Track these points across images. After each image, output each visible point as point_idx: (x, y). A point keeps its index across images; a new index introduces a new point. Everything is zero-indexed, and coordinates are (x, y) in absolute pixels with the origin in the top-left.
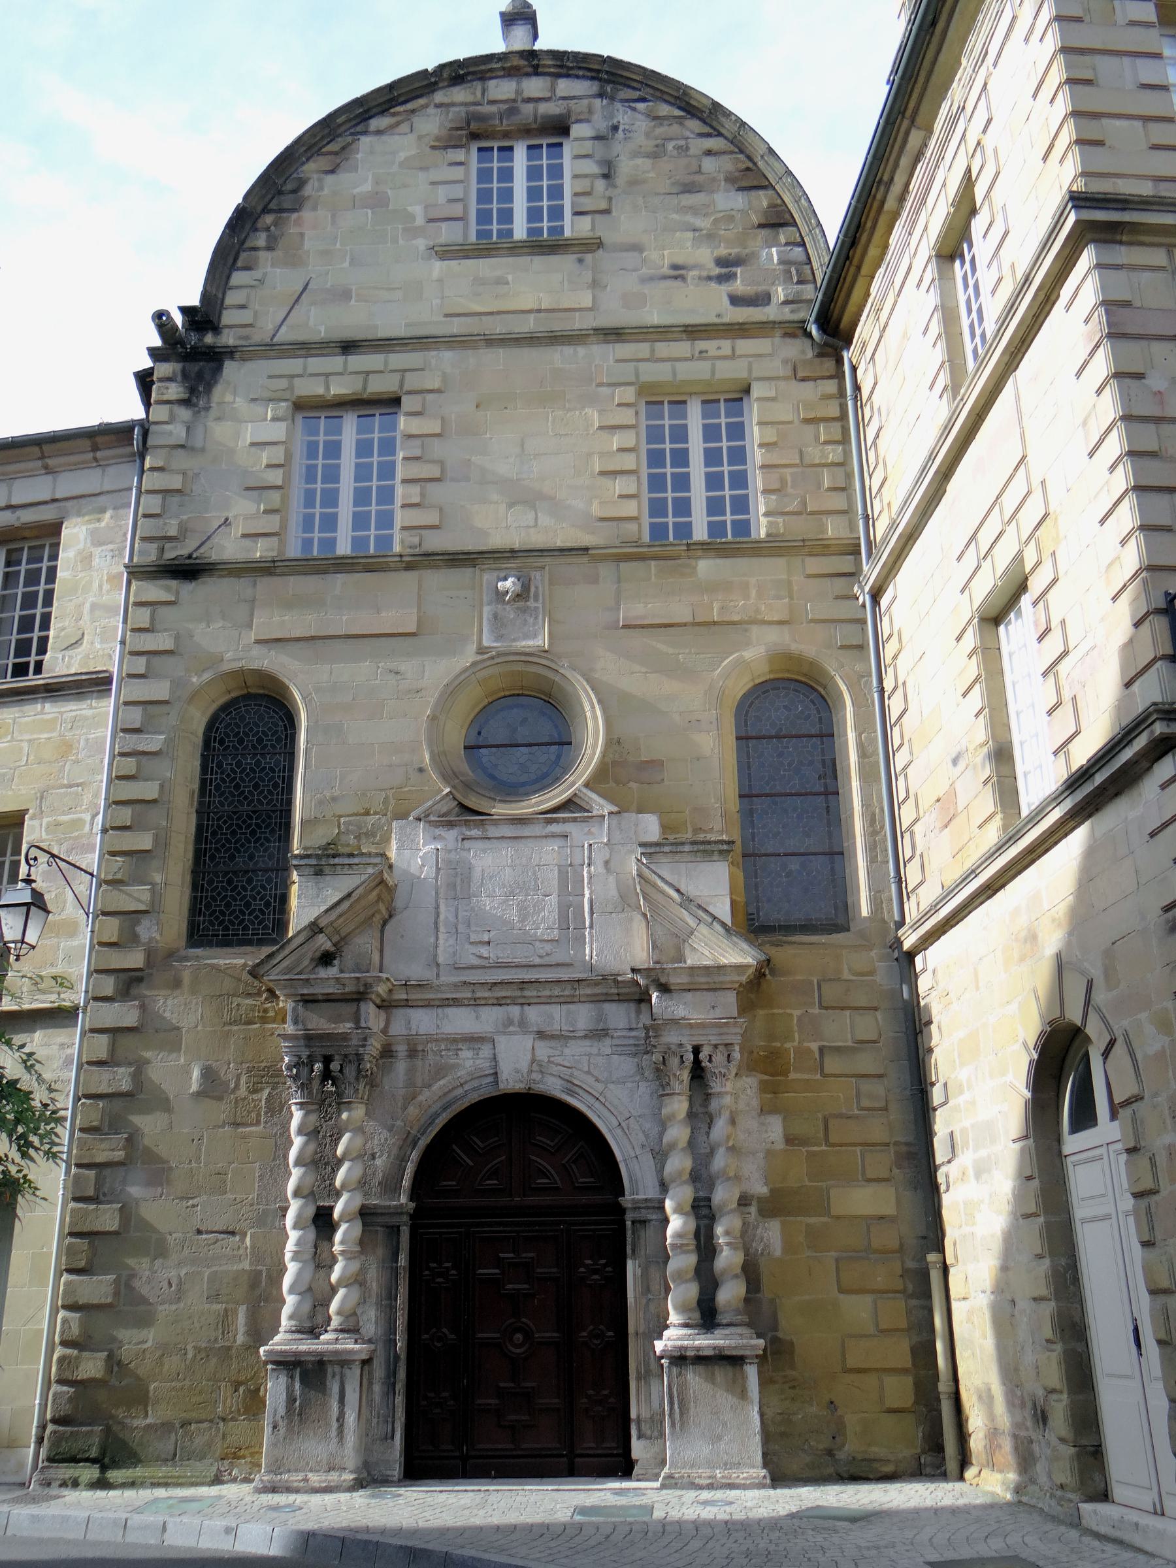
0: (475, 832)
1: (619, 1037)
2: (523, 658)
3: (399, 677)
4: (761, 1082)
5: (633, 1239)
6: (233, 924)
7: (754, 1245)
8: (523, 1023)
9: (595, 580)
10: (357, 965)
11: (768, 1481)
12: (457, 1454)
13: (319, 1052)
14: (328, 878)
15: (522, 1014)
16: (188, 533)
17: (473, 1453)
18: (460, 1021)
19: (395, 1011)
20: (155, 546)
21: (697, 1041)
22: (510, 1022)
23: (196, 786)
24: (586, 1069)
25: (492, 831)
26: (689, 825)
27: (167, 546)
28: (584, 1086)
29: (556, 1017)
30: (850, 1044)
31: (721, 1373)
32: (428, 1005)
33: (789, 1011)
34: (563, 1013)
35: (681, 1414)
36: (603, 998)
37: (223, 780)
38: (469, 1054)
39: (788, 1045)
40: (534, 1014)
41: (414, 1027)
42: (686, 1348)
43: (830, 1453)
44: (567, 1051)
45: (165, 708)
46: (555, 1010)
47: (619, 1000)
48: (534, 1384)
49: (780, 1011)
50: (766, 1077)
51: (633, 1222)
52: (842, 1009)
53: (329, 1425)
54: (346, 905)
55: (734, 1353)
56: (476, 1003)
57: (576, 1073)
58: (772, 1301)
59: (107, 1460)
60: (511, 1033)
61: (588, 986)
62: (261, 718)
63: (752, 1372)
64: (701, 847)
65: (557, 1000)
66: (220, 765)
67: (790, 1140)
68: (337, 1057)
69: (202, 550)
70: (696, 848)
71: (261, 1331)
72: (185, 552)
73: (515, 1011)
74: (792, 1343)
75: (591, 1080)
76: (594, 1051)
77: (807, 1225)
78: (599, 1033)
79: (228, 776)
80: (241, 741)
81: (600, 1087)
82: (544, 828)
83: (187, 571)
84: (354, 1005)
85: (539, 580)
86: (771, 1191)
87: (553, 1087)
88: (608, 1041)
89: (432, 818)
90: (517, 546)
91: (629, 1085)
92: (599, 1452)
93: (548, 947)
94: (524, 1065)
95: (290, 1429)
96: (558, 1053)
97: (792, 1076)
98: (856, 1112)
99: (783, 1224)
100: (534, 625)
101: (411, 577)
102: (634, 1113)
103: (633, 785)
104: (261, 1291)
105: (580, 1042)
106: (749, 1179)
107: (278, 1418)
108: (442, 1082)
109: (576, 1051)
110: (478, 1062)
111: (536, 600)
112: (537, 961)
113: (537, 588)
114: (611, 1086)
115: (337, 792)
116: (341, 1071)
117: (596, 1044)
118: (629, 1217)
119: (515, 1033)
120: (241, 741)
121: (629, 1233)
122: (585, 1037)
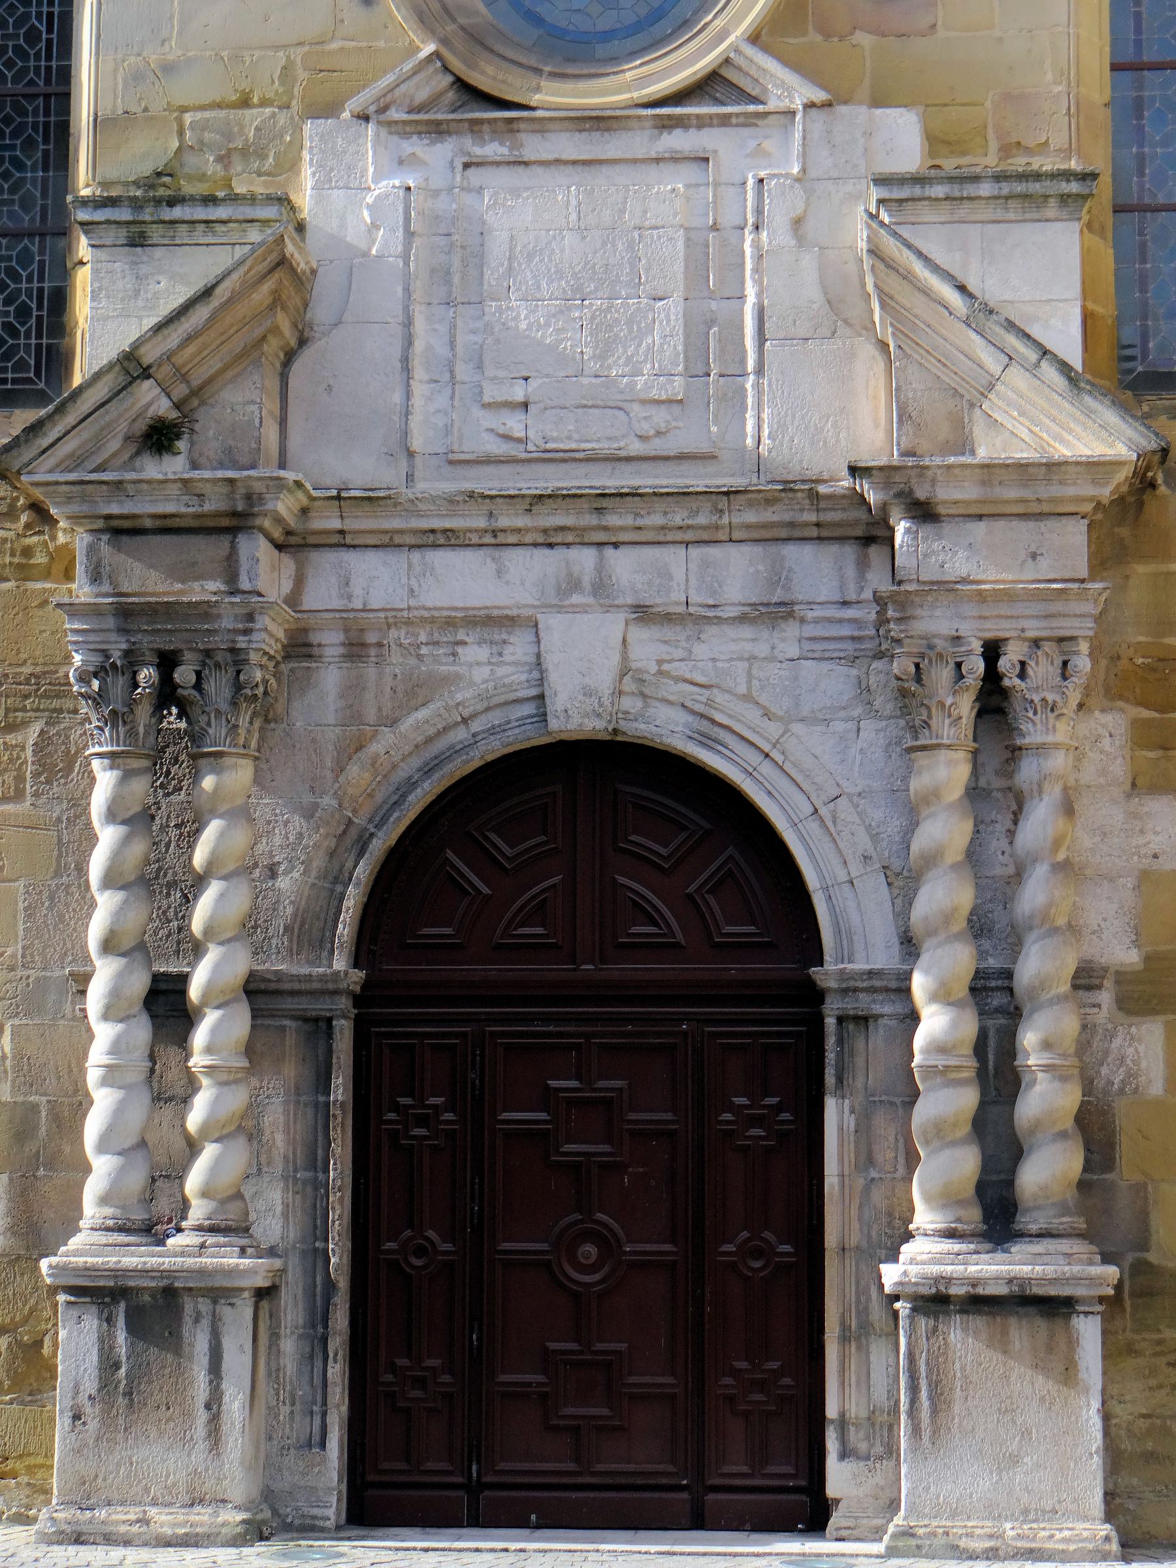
0: (493, 149)
1: (816, 621)
4: (1138, 725)
7: (1104, 1071)
8: (601, 587)
10: (229, 451)
11: (1115, 1547)
12: (459, 1480)
13: (147, 643)
14: (159, 252)
15: (600, 567)
17: (485, 1479)
18: (462, 580)
19: (315, 556)
22: (574, 585)
24: (742, 689)
29: (677, 573)
31: (1022, 1332)
32: (388, 543)
35: (935, 1411)
40: (625, 566)
41: (357, 590)
42: (949, 1280)
46: (675, 559)
47: (820, 539)
50: (1146, 714)
51: (840, 1020)
54: (201, 314)
55: (1053, 1292)
56: (496, 540)
57: (719, 698)
58: (1140, 1189)
61: (751, 504)
63: (1088, 1331)
64: (1020, 188)
65: (680, 536)
68: (188, 656)
70: (1006, 188)
73: (584, 559)
75: (753, 715)
76: (762, 649)
78: (774, 612)
81: (773, 729)
84: (225, 541)
86: (1148, 959)
87: (667, 728)
88: (792, 630)
89: (395, 114)
91: (839, 726)
93: (660, 417)
96: (680, 653)
99: (1167, 1024)
103: (864, 39)
105: (730, 631)
106: (1098, 932)
107: (83, 1398)
108: (422, 714)
109: (720, 649)
110: (501, 671)
112: (636, 448)
114: (797, 728)
116: (198, 686)
117: (765, 634)
118: (832, 1009)
119: (584, 609)
121: (831, 1042)
122: (742, 619)
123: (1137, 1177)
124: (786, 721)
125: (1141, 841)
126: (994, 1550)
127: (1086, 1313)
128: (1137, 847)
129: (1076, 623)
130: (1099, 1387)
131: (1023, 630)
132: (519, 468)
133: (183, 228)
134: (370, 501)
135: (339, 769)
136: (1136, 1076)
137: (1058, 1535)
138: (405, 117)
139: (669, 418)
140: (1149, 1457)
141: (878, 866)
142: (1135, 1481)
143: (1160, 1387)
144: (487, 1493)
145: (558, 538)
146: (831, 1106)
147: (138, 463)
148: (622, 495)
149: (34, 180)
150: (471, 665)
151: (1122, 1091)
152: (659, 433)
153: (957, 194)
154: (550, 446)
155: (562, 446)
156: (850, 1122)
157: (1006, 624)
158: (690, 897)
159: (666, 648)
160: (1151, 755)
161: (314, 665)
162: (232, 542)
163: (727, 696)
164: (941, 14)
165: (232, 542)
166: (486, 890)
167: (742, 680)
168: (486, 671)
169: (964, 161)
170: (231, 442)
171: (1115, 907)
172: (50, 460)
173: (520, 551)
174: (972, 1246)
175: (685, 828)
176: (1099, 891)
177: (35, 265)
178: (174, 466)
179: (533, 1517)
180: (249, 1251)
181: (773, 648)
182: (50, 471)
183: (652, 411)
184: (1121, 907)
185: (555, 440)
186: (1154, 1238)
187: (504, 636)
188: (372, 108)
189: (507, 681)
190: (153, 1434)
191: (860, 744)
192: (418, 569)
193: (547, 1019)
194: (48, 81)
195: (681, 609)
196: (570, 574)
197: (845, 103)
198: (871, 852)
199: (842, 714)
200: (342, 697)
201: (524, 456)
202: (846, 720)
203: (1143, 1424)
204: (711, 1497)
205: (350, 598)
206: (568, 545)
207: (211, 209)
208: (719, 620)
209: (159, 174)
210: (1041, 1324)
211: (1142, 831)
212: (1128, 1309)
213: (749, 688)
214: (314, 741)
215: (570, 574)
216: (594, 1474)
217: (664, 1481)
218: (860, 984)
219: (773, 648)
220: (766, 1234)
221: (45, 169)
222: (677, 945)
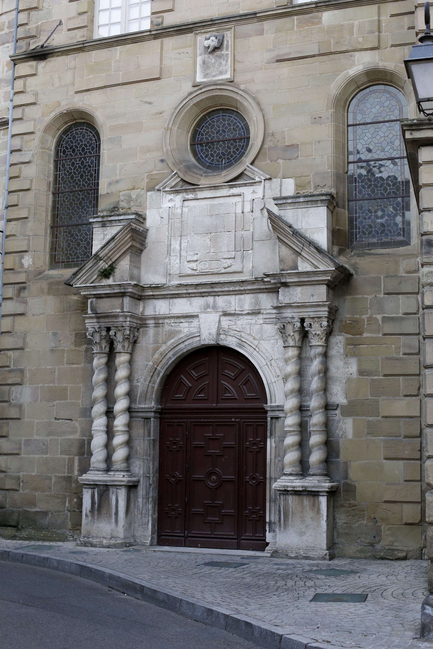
0: (191, 196)
1: (267, 314)
2: (219, 87)
3: (151, 106)
4: (347, 339)
5: (271, 426)
6: (71, 255)
7: (337, 432)
8: (215, 307)
9: (261, 33)
10: (122, 277)
11: (328, 557)
12: (183, 535)
13: (103, 325)
14: (108, 228)
15: (214, 302)
16: (42, 33)
17: (189, 535)
18: (181, 306)
19: (148, 301)
20: (25, 42)
21: (304, 315)
22: (208, 306)
23: (51, 179)
24: (248, 332)
25: (201, 195)
26: (312, 183)
27: (32, 41)
28: (248, 342)
29: (233, 303)
30: (400, 315)
31: (306, 501)
32: (164, 297)
33: (365, 296)
34: (237, 301)
35: (285, 521)
36: (258, 291)
37: (65, 174)
38: (186, 325)
39: (364, 317)
40: (221, 301)
41: (157, 310)
42: (288, 487)
43: (372, 545)
44: (239, 323)
45: (32, 136)
46: (232, 299)
47: (268, 292)
48: (221, 502)
49: (360, 296)
50: (350, 336)
51: (272, 418)
52: (398, 294)
53: (110, 516)
54: (112, 244)
55: (314, 489)
56: (189, 295)
57: (243, 334)
58: (346, 463)
59: (20, 526)
60: (208, 313)
61: (248, 284)
62: (84, 136)
63: (323, 500)
64: (310, 199)
65: (233, 293)
66: (63, 166)
67: (361, 373)
68: (112, 328)
69: (48, 42)
70: (307, 199)
71: (85, 468)
72: (40, 44)
73: (210, 299)
74: (355, 487)
75: (251, 339)
76: (253, 321)
77: (369, 421)
78: (256, 313)
79: (68, 171)
80: (74, 151)
81: (256, 342)
82: (229, 191)
83: (41, 55)
84: (121, 299)
85: (229, 36)
86: (349, 402)
87: (231, 342)
88: (261, 316)
89: (167, 189)
90: (214, 17)
91: (272, 341)
92: (212, 536)
93: (229, 262)
94: (214, 331)
95: (93, 516)
96: (233, 323)
97: (365, 335)
98: (401, 356)
99: (354, 419)
100: (226, 65)
101: (158, 42)
102: (275, 357)
103: (280, 161)
104: (84, 450)
105: (246, 317)
106: (336, 395)
107: (88, 512)
108: (172, 341)
109: (243, 321)
110: (191, 329)
111: (227, 50)
112: (223, 271)
113: (228, 42)
114: (262, 342)
115: (118, 178)
116: (115, 336)
117: (254, 318)
118: (270, 414)
119: (211, 312)
120: (74, 151)
121: (269, 424)
122: (248, 314)
123: (345, 460)
124: (259, 340)
125: (347, 370)
126: (297, 556)
127: (323, 496)
128: (347, 372)
129: (323, 313)
130: (326, 515)
131: (310, 315)
132: (195, 277)
133: (113, 222)
134: (157, 288)
135: (153, 355)
136: (345, 433)
137: (314, 553)
138: (169, 189)
139: (231, 262)
140: (347, 534)
141: (281, 378)
142: (343, 540)
143: (350, 515)
144: (189, 539)
145: (204, 295)
146: (268, 440)
147: (101, 281)
148: (217, 283)
149: (91, 210)
150: (184, 328)
151: (341, 437)
152: (229, 267)
153: (295, 201)
154: (203, 271)
155: (205, 271)
156: (274, 445)
157: (305, 314)
158: (239, 386)
159: (230, 322)
160: (351, 347)
161: (148, 329)
162: (123, 300)
163: (245, 334)
164: (300, 153)
165: (123, 300)
166: (190, 385)
167: (248, 330)
168: (187, 329)
169: (305, 191)
170: (122, 275)
171: (340, 388)
172: (80, 282)
173: (195, 298)
174: (295, 478)
175: (238, 368)
176: (337, 384)
177: (91, 232)
178: (110, 281)
179: (199, 545)
180: (126, 476)
181: (256, 321)
182: (80, 284)
183: (227, 260)
184: (342, 388)
185: (204, 269)
186: (349, 476)
187: (192, 320)
188: (162, 188)
189: (192, 332)
190: (103, 520)
191: (277, 346)
192: (171, 304)
193: (205, 418)
194: (95, 186)
195: (233, 312)
196: (207, 304)
197: (276, 178)
198: (279, 374)
199: (273, 338)
200: (154, 337)
201: (196, 274)
202: (274, 340)
203: (345, 525)
204: (242, 541)
205: (155, 312)
206: (207, 296)
207: (119, 217)
208: (242, 315)
209: (114, 208)
210: (311, 498)
211: (348, 367)
212: (342, 495)
213: (250, 332)
214: (147, 348)
215: (207, 304)
216: (165, 532)
217: (231, 537)
218: (276, 409)
219: (256, 321)
220: (257, 474)
221: (94, 208)
222: (236, 399)
